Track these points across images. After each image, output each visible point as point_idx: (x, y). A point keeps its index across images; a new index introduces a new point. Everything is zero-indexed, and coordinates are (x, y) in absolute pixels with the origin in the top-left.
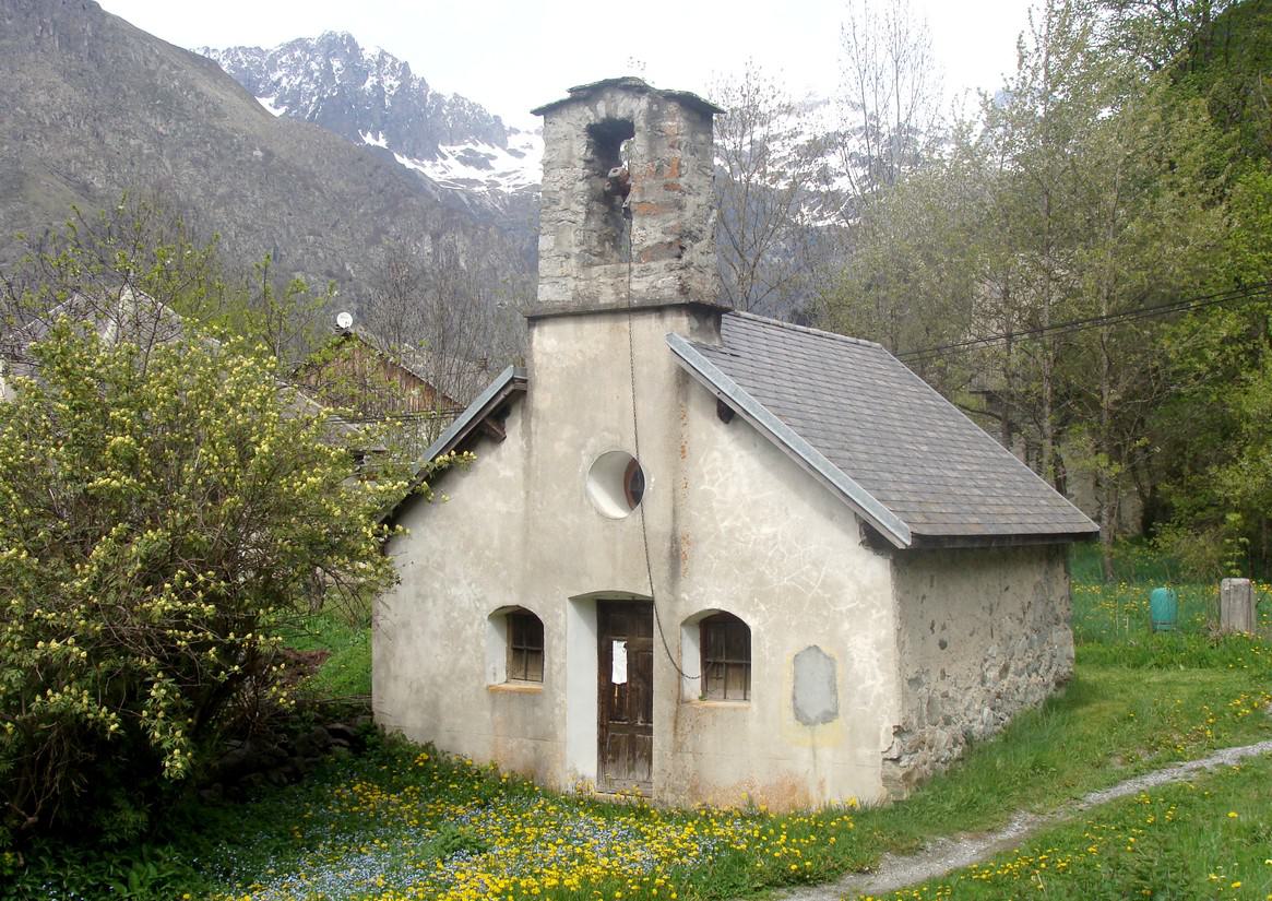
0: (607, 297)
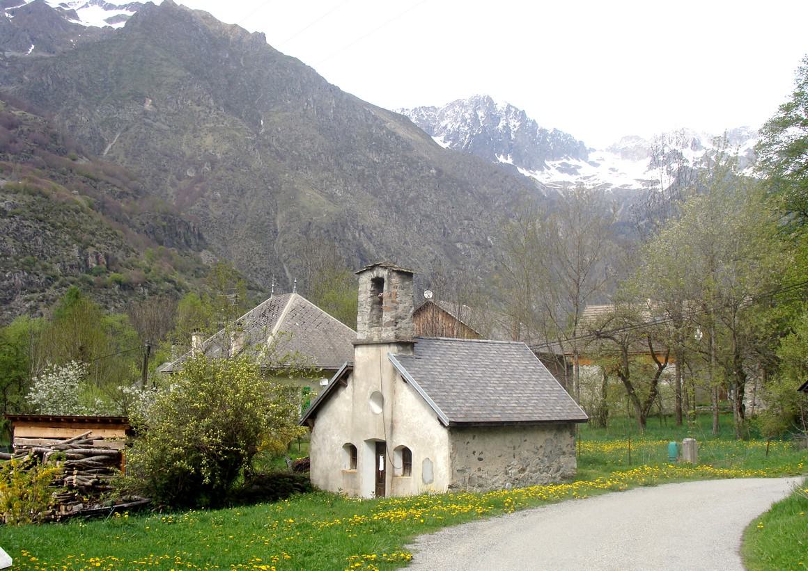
0: (376, 339)
